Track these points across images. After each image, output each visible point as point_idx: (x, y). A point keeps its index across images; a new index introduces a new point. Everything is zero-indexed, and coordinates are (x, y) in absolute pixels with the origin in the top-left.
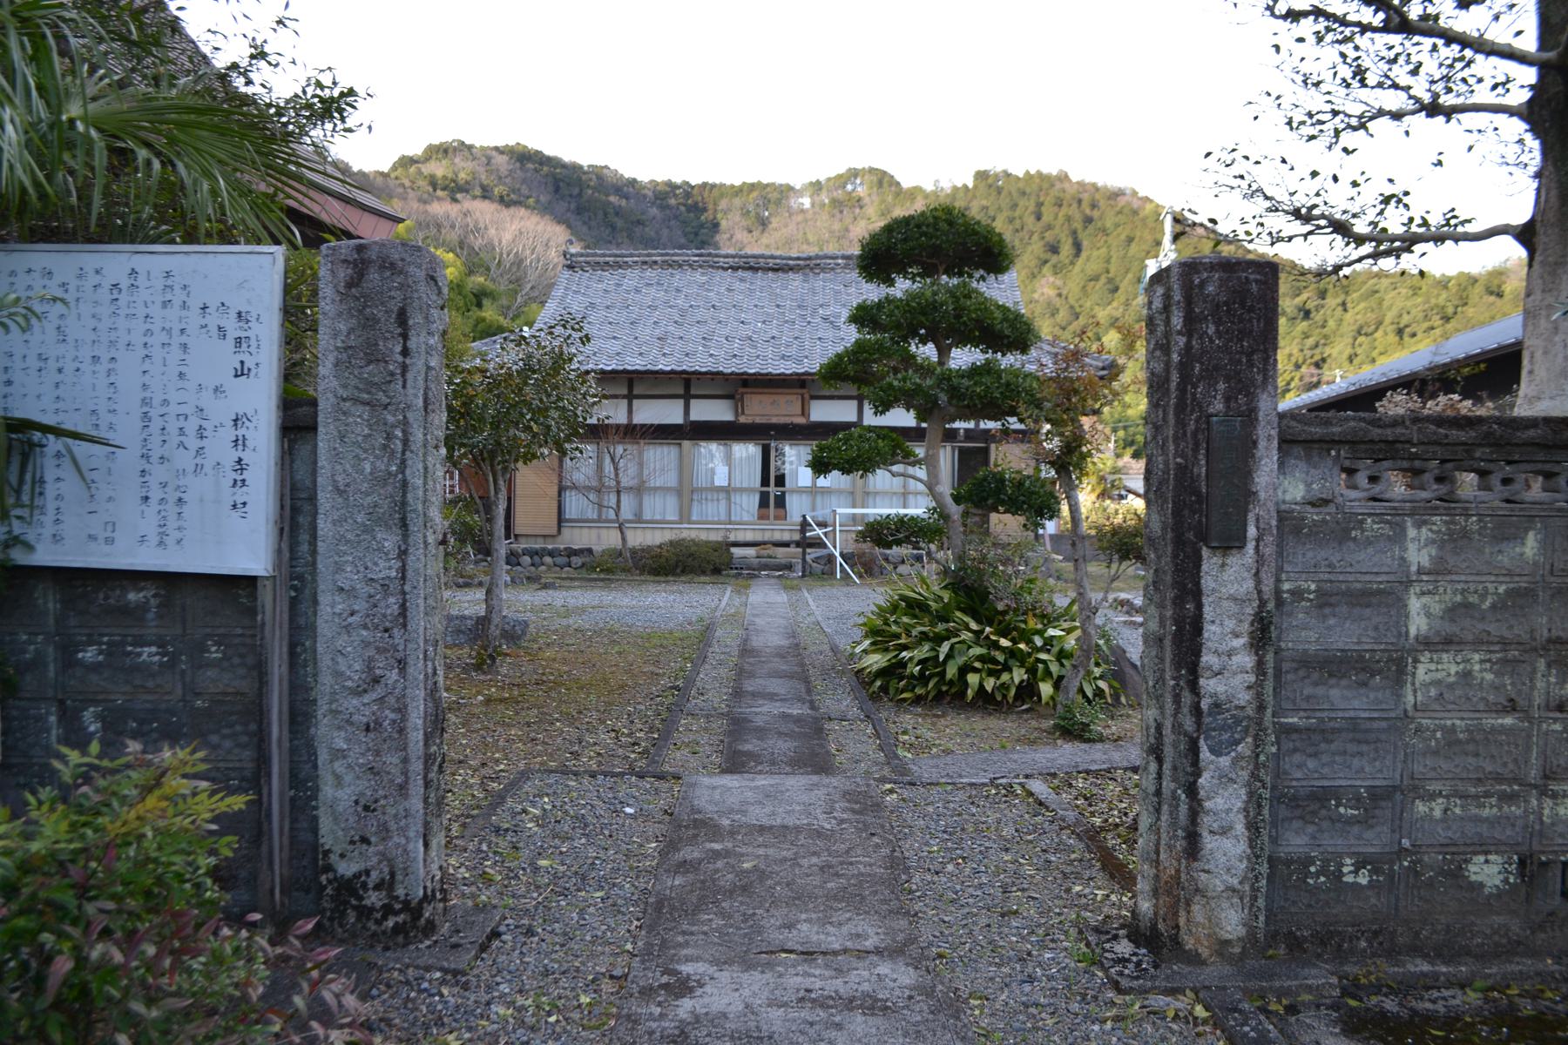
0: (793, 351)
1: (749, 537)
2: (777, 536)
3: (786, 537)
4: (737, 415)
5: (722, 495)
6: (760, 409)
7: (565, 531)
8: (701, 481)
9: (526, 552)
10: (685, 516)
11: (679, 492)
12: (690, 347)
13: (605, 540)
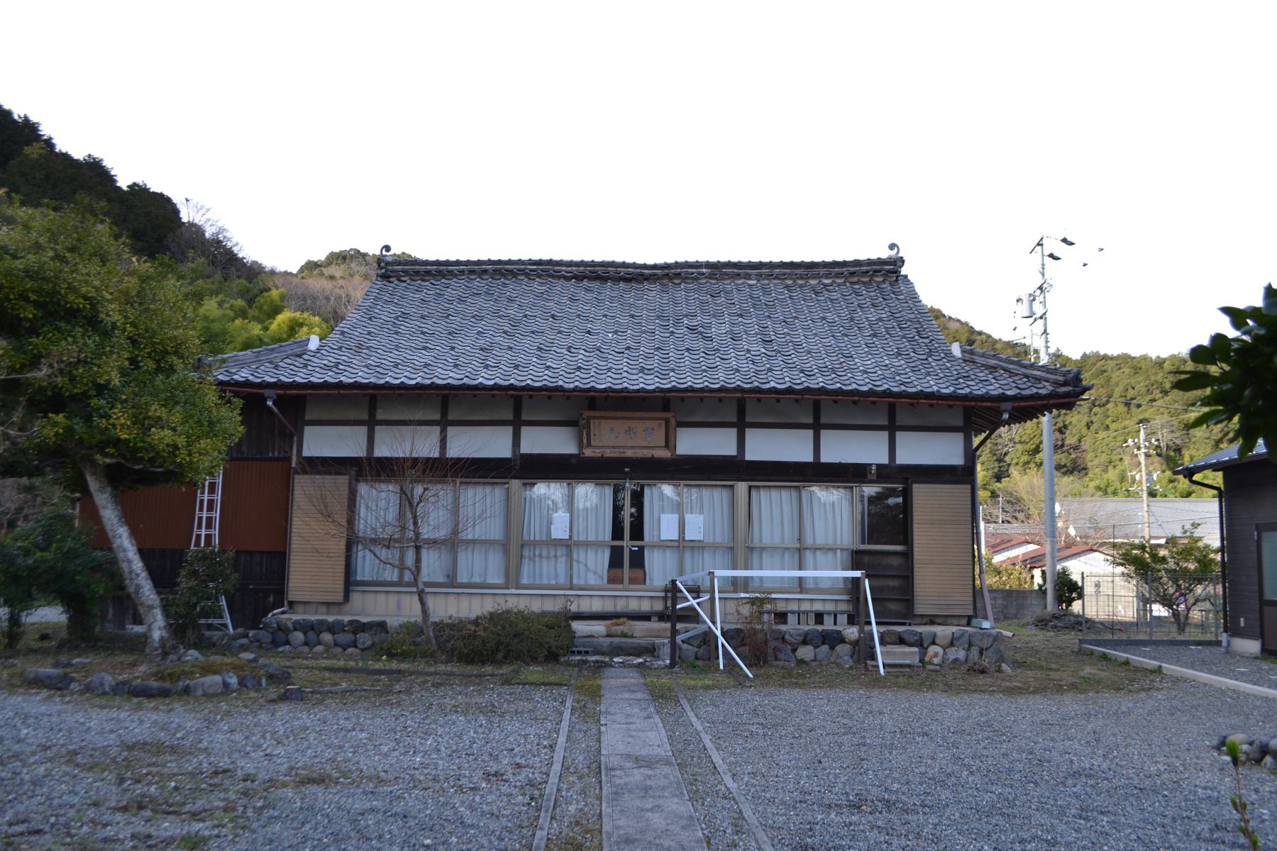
0: (654, 363)
1: (597, 606)
2: (634, 606)
3: (645, 606)
4: (581, 446)
5: (561, 551)
6: (614, 438)
7: (356, 598)
8: (534, 531)
9: (298, 626)
10: (512, 578)
11: (505, 546)
12: (521, 359)
13: (396, 610)
